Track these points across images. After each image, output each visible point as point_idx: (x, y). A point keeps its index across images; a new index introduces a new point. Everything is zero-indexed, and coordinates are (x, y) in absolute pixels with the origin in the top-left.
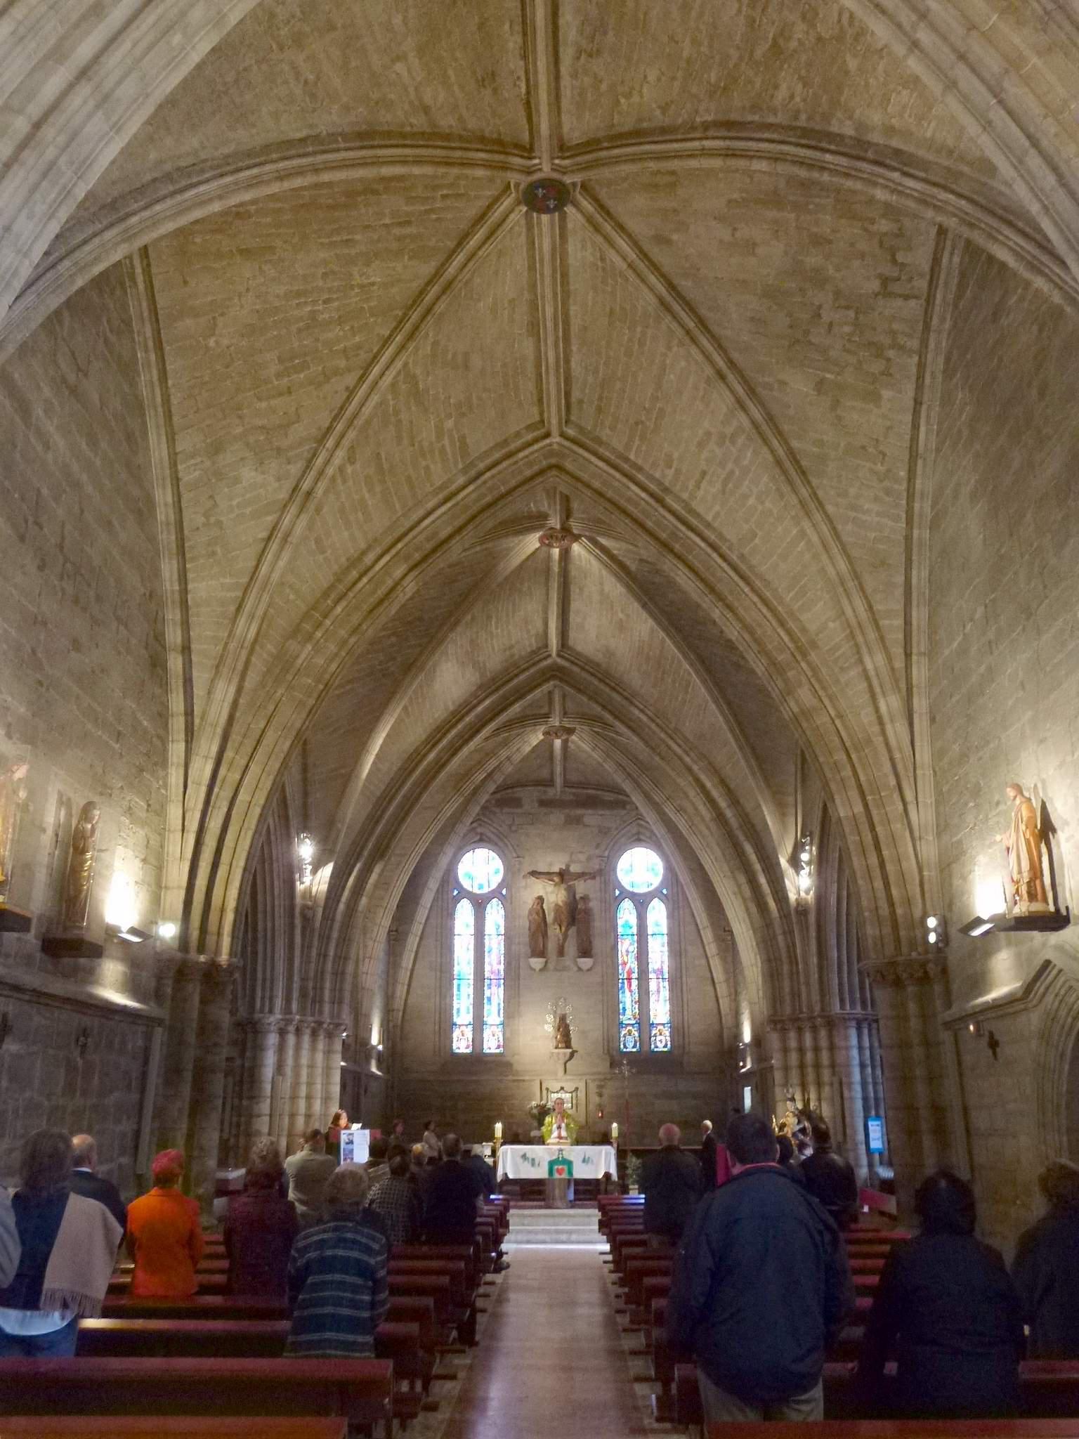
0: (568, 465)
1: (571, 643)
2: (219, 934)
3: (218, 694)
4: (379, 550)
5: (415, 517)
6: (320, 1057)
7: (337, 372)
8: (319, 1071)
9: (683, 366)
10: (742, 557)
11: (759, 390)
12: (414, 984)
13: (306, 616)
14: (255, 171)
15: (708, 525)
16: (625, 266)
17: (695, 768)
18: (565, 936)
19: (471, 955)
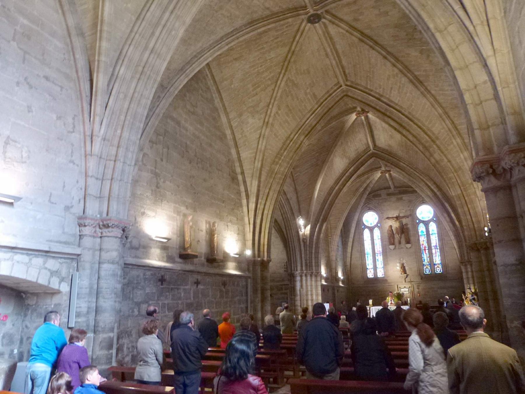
0: (349, 94)
1: (377, 144)
2: (264, 252)
3: (253, 184)
4: (294, 133)
5: (304, 121)
6: (313, 283)
7: (268, 86)
8: (314, 287)
9: (374, 56)
10: (409, 113)
11: (400, 59)
12: (353, 257)
13: (276, 157)
14: (219, 45)
15: (397, 104)
16: (345, 32)
17: (424, 180)
18: (401, 238)
19: (370, 246)
